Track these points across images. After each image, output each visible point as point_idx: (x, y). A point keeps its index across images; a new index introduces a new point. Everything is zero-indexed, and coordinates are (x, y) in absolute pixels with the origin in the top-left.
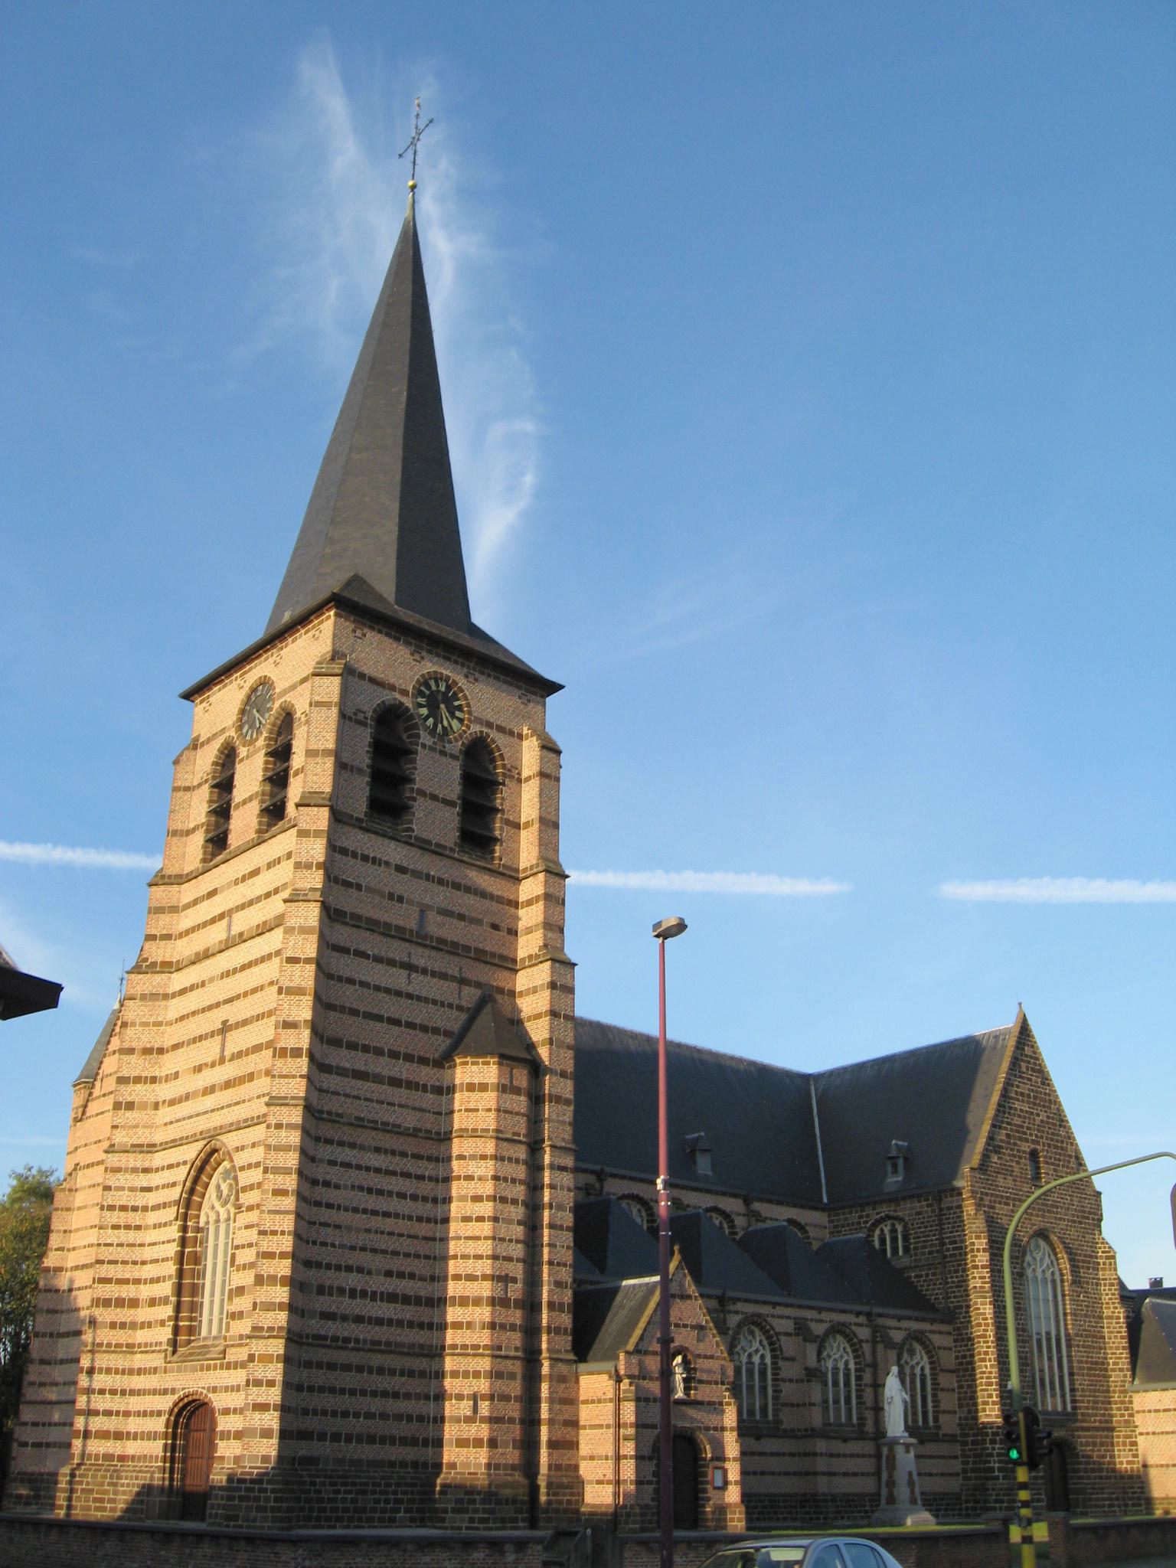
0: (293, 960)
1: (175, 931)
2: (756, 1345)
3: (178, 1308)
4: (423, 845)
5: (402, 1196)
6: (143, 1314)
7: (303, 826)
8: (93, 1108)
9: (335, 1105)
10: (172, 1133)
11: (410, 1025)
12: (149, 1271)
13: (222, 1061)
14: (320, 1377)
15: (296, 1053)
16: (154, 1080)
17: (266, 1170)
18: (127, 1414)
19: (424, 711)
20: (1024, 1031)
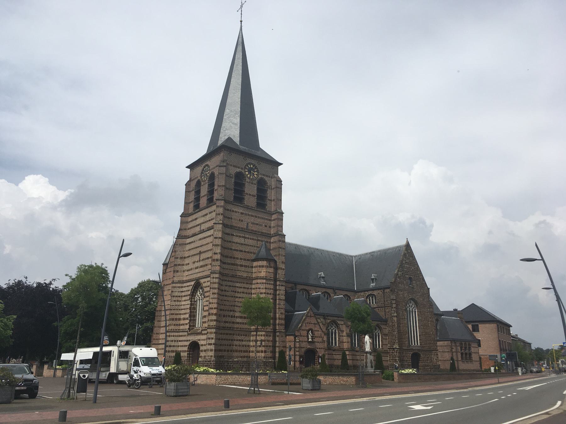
0: (216, 238)
1: (187, 228)
2: (334, 327)
3: (190, 321)
4: (247, 207)
5: (243, 293)
6: (182, 322)
7: (217, 204)
8: (168, 270)
9: (226, 272)
10: (188, 278)
11: (245, 252)
12: (183, 312)
13: (200, 261)
14: (224, 337)
15: (217, 260)
16: (183, 265)
17: (211, 283)
18: (178, 346)
19: (247, 173)
20: (408, 246)
